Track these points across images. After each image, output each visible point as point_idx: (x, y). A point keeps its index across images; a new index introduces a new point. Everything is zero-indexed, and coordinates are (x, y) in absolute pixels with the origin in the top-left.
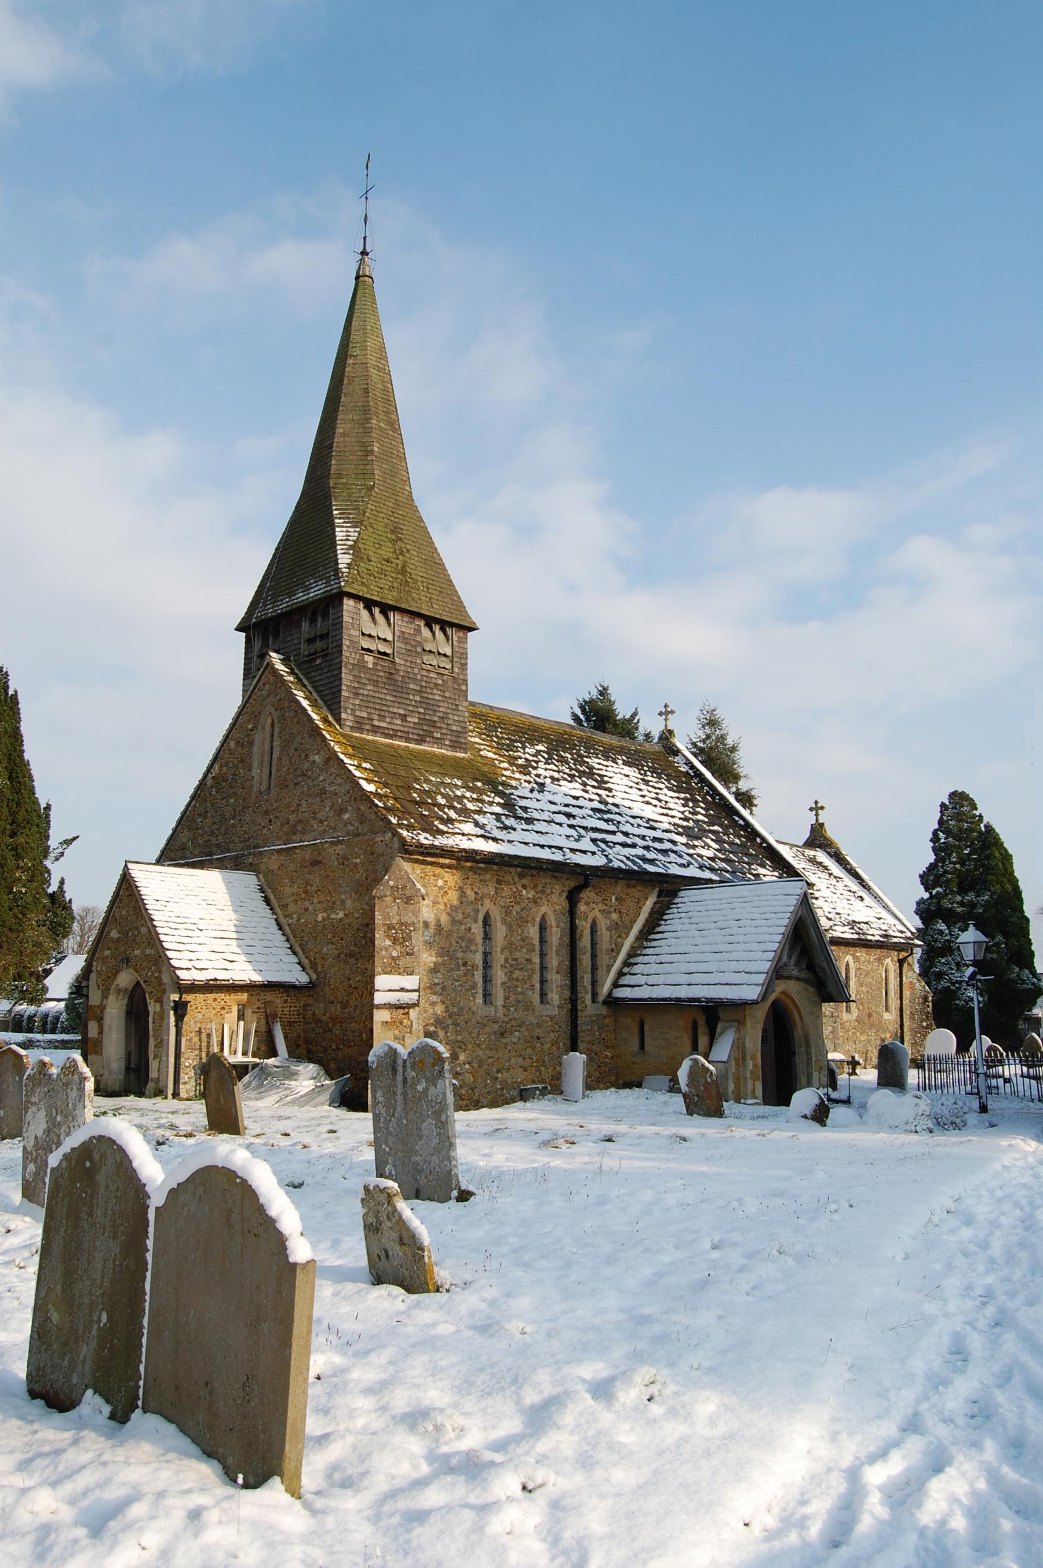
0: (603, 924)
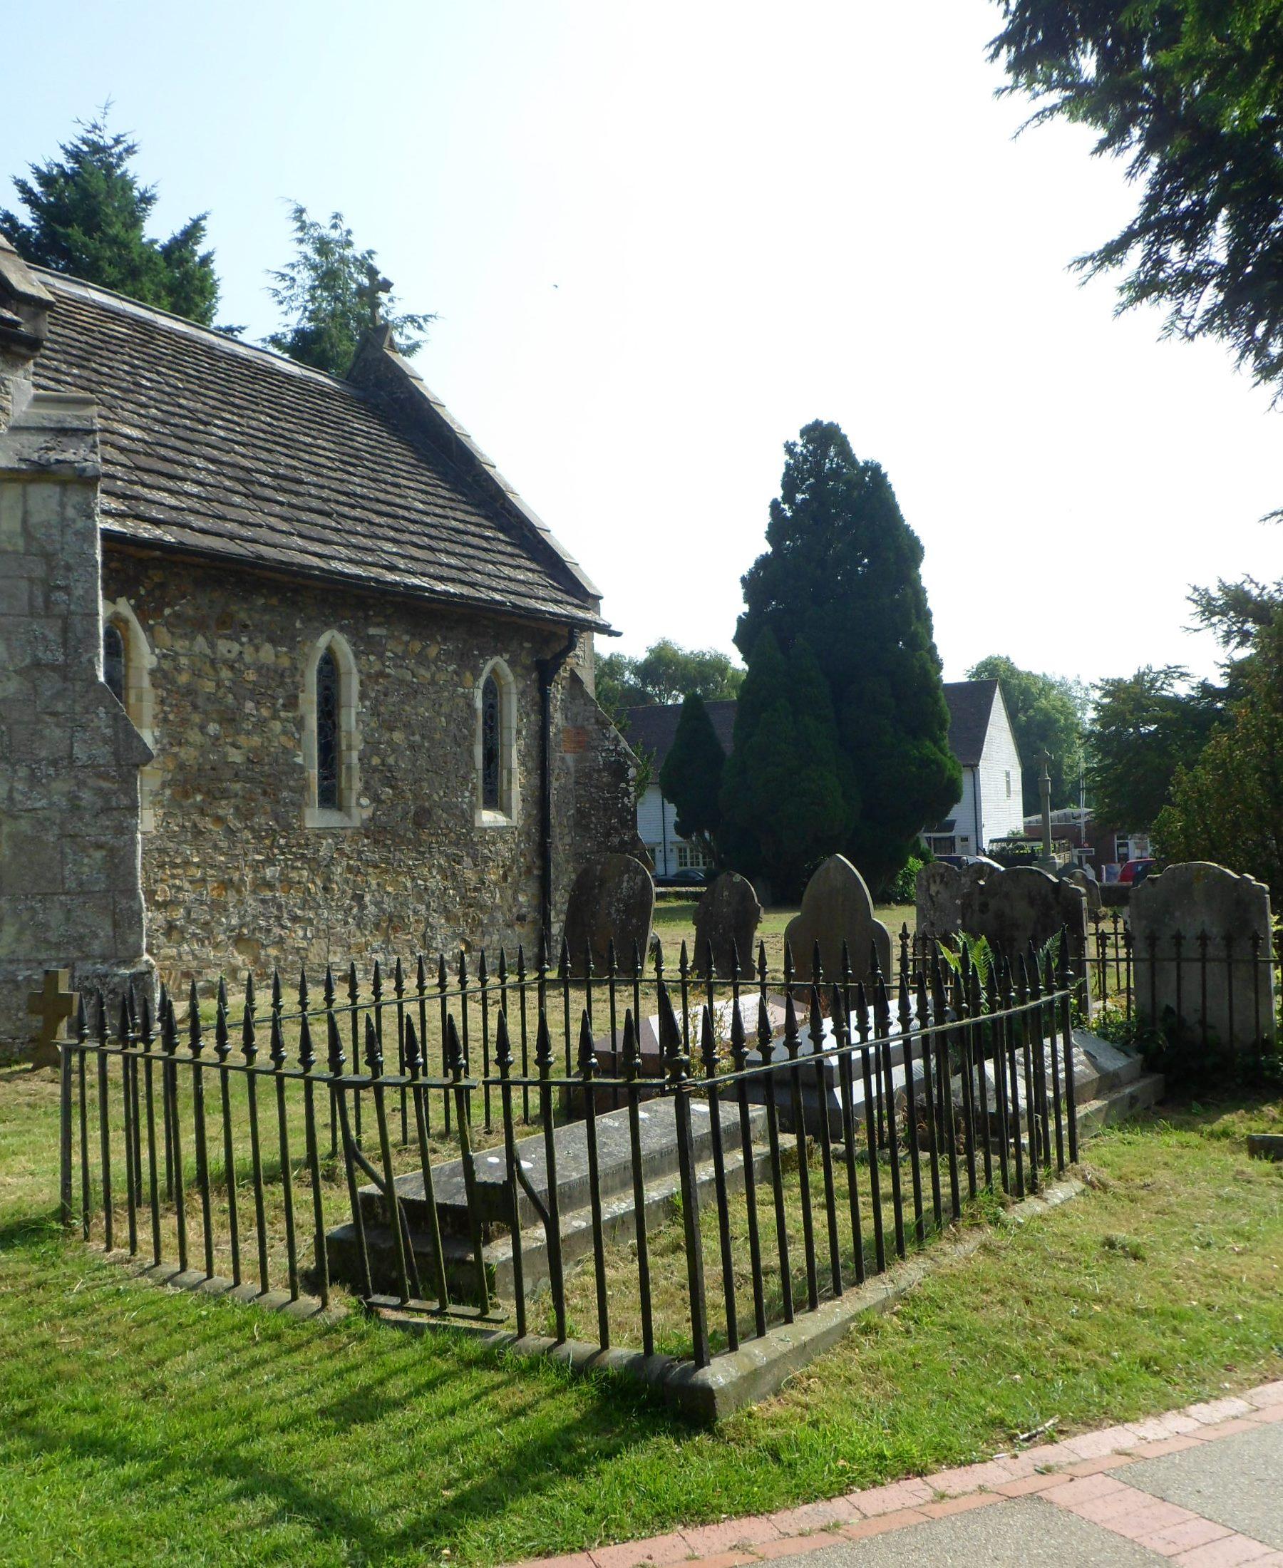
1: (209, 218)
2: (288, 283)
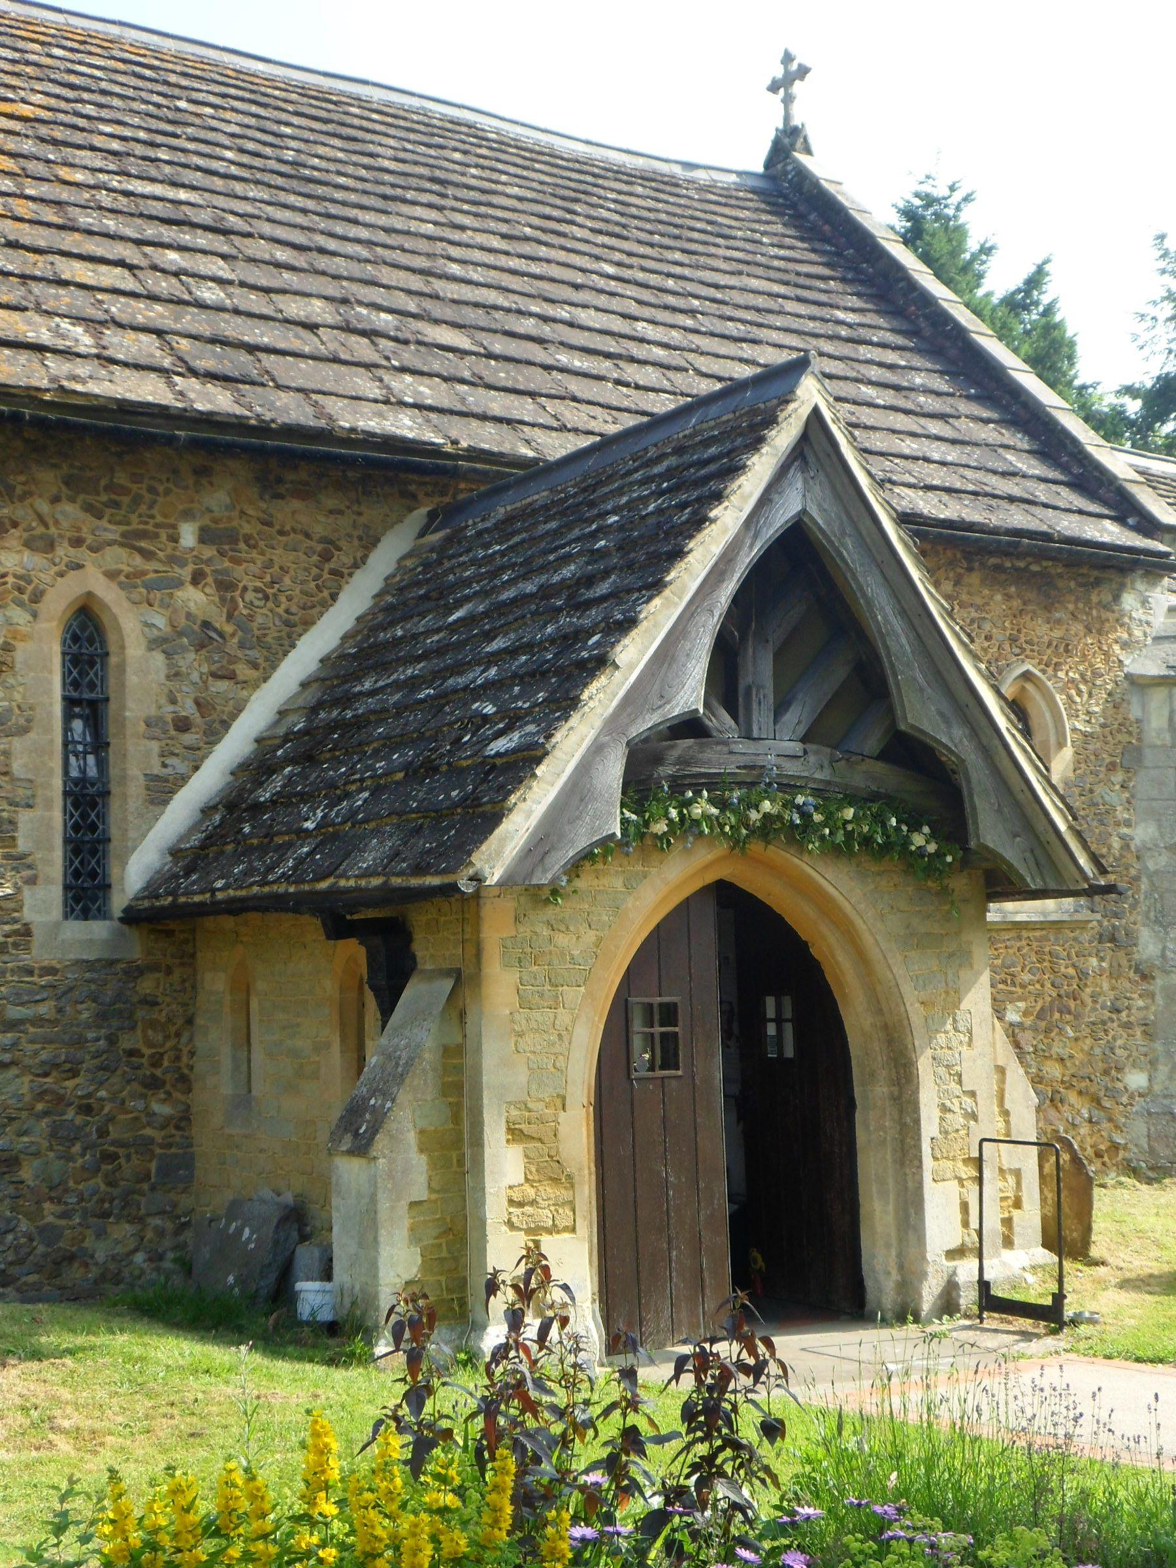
0: (132, 627)
1: (793, 51)
2: (1150, 323)
